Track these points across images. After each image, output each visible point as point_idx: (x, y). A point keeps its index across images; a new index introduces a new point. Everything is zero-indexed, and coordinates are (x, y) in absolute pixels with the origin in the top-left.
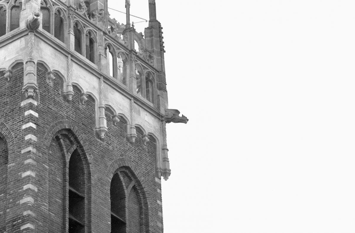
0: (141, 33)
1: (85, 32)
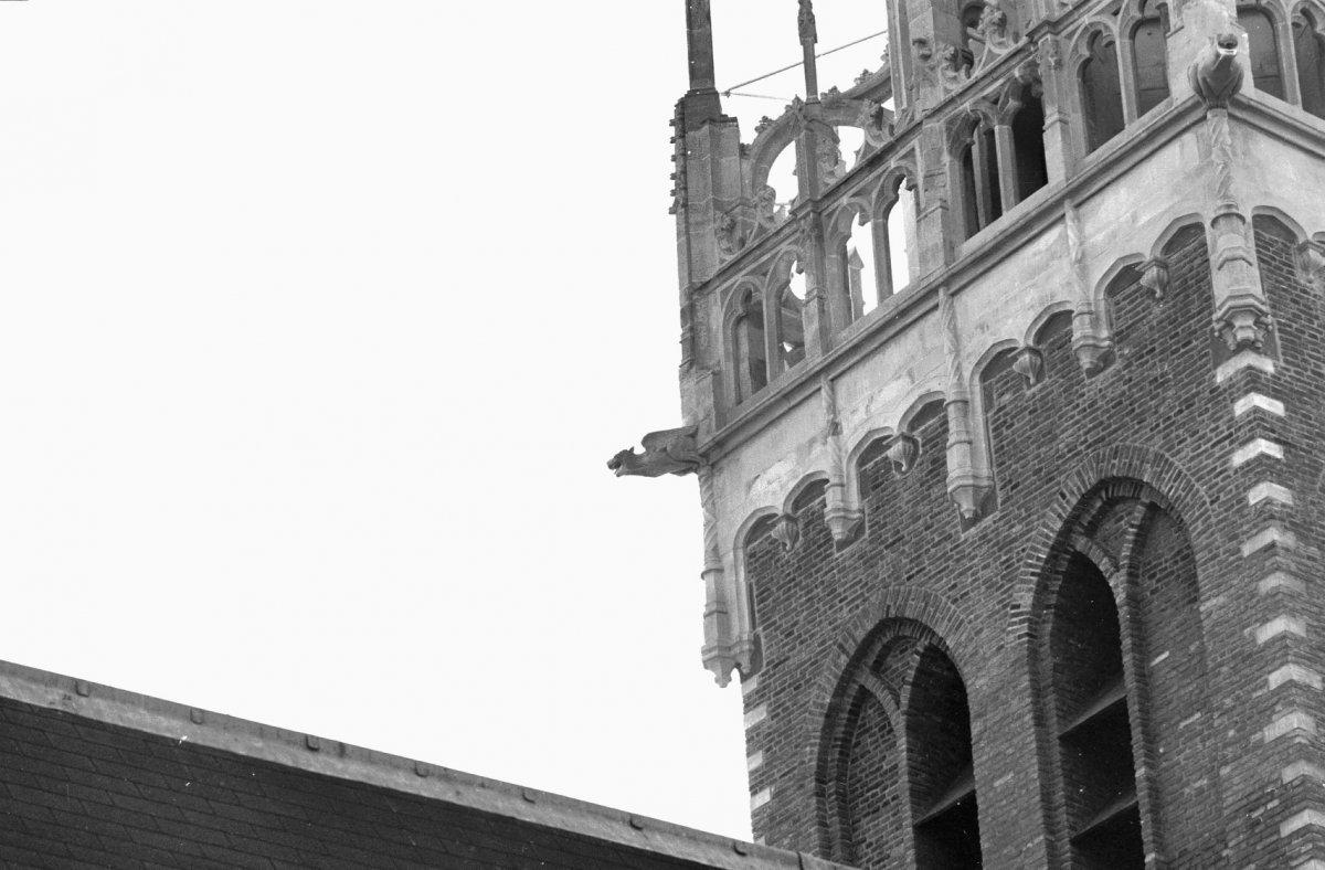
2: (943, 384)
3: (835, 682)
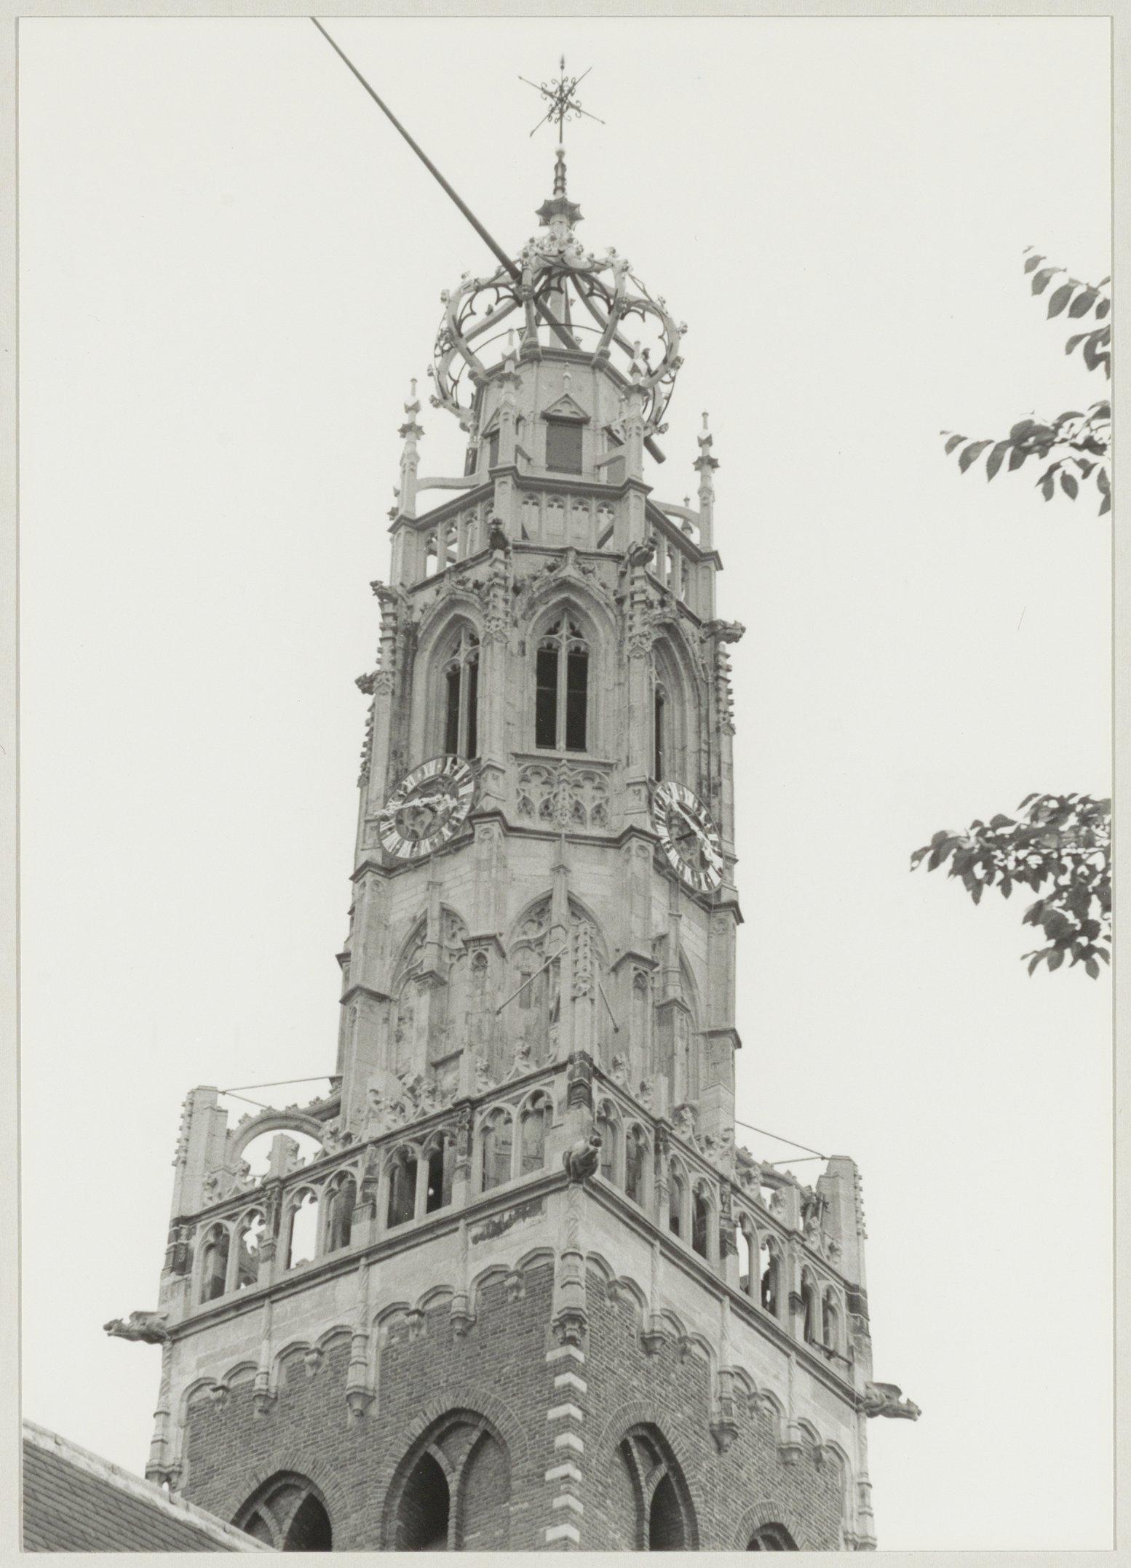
0: (810, 1187)
1: (625, 1127)
2: (349, 1319)
3: (238, 1506)
